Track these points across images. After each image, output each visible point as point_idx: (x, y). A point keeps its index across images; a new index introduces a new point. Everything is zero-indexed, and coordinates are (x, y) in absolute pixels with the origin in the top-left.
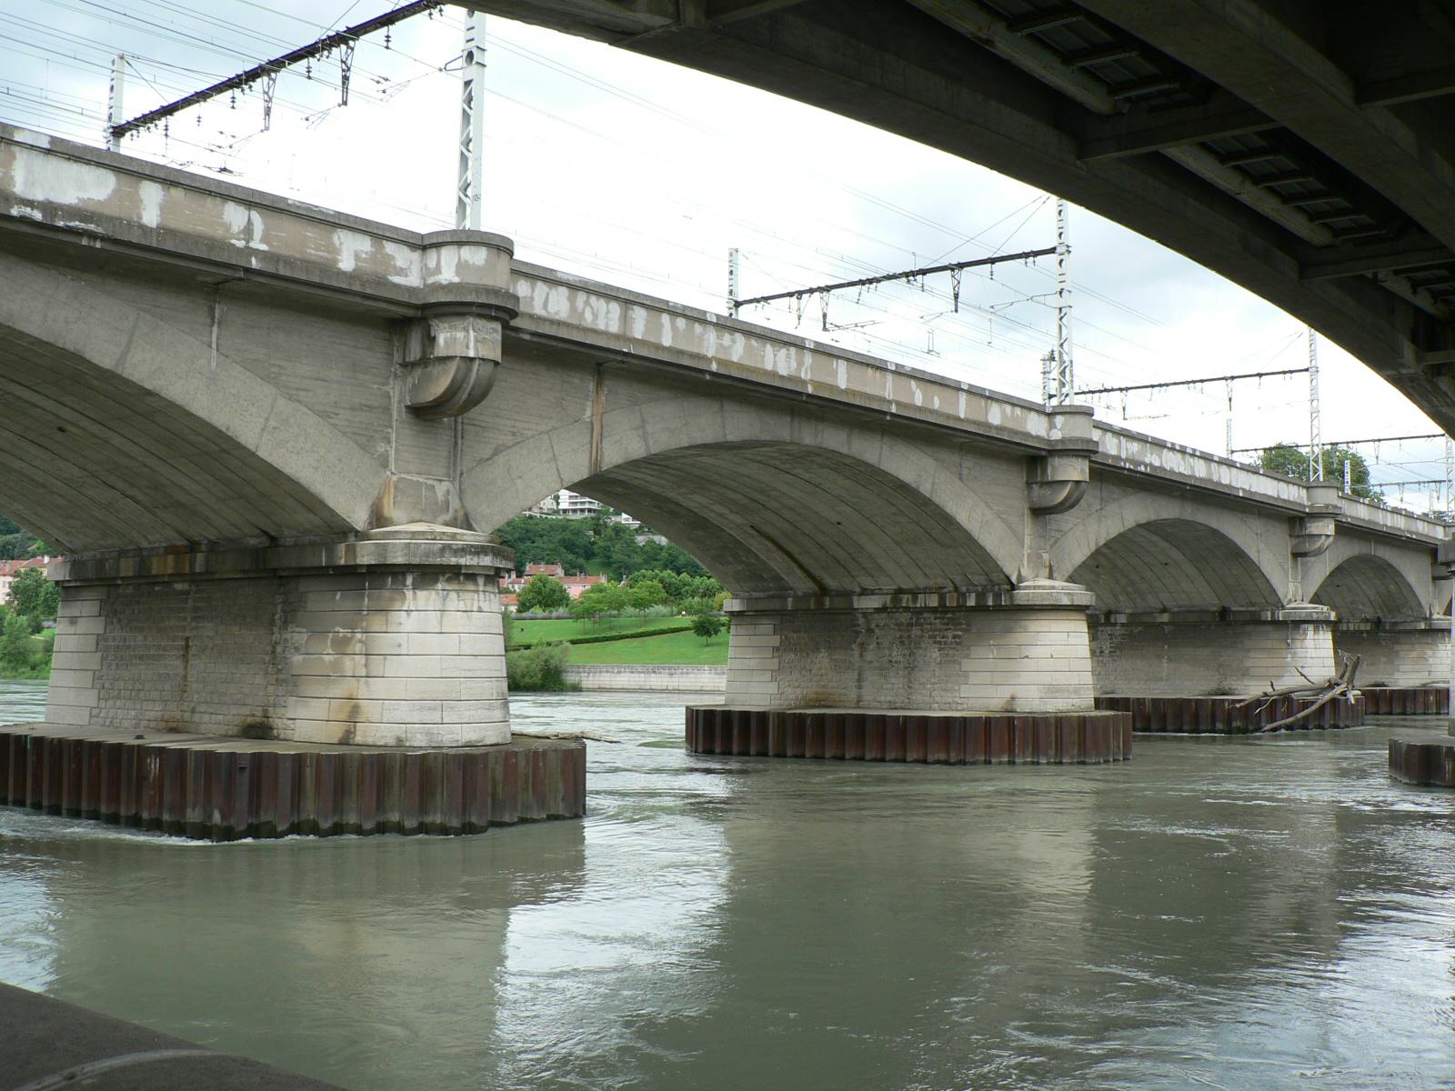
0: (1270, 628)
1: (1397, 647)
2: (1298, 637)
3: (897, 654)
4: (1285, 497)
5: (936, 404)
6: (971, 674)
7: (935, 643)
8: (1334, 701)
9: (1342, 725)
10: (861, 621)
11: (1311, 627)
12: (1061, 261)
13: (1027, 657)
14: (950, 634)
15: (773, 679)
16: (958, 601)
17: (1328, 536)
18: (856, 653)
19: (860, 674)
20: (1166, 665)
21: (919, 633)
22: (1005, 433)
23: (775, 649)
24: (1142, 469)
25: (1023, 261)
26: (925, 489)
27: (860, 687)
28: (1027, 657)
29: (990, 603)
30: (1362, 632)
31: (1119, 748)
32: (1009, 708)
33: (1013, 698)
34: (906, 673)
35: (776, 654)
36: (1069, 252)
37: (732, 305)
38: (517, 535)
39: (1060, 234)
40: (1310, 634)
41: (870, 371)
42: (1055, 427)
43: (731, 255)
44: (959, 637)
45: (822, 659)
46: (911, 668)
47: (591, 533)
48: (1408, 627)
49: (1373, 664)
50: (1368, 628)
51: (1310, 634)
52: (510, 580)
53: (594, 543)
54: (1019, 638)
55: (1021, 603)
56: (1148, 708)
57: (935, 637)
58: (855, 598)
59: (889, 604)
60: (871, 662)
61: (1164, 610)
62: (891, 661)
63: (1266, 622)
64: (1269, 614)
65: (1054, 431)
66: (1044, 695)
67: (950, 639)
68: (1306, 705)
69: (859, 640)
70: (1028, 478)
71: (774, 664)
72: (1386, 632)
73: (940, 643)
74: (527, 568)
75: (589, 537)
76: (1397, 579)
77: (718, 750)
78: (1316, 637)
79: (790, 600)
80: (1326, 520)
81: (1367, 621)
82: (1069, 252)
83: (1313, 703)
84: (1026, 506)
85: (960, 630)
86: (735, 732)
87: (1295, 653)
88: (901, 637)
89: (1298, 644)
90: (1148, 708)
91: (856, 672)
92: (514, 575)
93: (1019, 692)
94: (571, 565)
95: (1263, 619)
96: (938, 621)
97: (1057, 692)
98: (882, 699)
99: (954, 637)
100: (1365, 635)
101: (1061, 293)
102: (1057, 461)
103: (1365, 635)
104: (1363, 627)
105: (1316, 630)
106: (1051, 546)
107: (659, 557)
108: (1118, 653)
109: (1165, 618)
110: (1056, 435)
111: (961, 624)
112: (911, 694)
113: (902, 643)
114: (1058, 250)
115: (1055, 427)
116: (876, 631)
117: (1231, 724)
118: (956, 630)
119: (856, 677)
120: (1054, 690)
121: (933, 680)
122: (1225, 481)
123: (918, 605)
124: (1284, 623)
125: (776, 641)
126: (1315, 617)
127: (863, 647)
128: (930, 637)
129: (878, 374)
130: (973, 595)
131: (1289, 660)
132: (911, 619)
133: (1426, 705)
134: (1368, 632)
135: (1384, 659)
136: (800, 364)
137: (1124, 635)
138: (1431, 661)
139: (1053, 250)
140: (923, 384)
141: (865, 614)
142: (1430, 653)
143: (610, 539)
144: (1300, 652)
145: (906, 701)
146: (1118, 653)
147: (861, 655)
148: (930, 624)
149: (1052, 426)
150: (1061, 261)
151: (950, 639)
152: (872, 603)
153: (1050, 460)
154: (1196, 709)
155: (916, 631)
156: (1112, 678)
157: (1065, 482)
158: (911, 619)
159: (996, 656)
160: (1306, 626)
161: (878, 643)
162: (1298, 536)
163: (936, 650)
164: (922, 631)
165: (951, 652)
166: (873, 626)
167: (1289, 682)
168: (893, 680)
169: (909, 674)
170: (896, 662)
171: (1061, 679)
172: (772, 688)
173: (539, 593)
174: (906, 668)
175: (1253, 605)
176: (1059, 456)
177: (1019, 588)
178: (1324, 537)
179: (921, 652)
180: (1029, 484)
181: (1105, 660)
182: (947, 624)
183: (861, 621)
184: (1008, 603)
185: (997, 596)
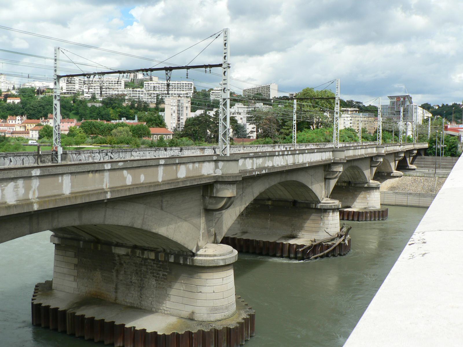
0: (314, 211)
1: (356, 193)
2: (326, 215)
3: (134, 279)
4: (324, 158)
5: (142, 179)
6: (171, 296)
7: (153, 276)
8: (340, 244)
9: (342, 254)
10: (117, 258)
11: (331, 211)
12: (225, 72)
13: (201, 292)
14: (161, 273)
15: (75, 280)
16: (165, 258)
17: (340, 172)
18: (114, 274)
19: (116, 285)
20: (269, 222)
21: (145, 270)
22: (188, 182)
23: (76, 265)
24: (264, 172)
25: (204, 69)
26: (138, 224)
27: (116, 292)
28: (201, 292)
29: (182, 262)
30: (343, 186)
31: (248, 334)
32: (191, 318)
33: (193, 313)
34: (139, 289)
35: (76, 268)
36: (229, 67)
37: (56, 77)
38: (45, 103)
39: (225, 44)
40: (331, 214)
41: (91, 175)
42: (218, 168)
43: (55, 50)
44: (165, 275)
45: (98, 275)
46: (141, 288)
47: (72, 102)
48: (360, 186)
49: (346, 199)
50: (346, 185)
51: (331, 214)
52: (42, 121)
53: (73, 106)
54: (197, 281)
55: (198, 265)
56: (262, 245)
57: (153, 273)
58: (113, 247)
59: (130, 253)
60: (121, 280)
61: (269, 199)
62: (131, 282)
63: (313, 208)
64: (314, 205)
65: (217, 170)
66: (209, 312)
67: (161, 276)
68: (328, 247)
69: (115, 268)
70: (203, 193)
71: (75, 273)
72: (352, 187)
73: (156, 277)
74: (49, 116)
75: (71, 104)
76: (359, 170)
77: (43, 326)
78: (333, 215)
79: (81, 242)
80: (340, 165)
81: (345, 182)
82: (229, 67)
83: (331, 246)
84: (202, 207)
85: (167, 272)
86: (51, 318)
87: (324, 222)
88: (136, 270)
89: (326, 218)
90: (262, 245)
91: (115, 284)
92: (43, 119)
93: (197, 310)
94: (65, 114)
95: (311, 207)
96: (155, 265)
97: (216, 310)
98: (128, 301)
99: (163, 275)
100: (344, 187)
101: (224, 90)
102: (219, 186)
103: (344, 187)
104: (343, 184)
105: (333, 212)
106: (216, 223)
107: (96, 111)
108: (249, 215)
109: (270, 203)
110: (219, 173)
111: (166, 269)
112: (141, 301)
113: (137, 273)
114: (224, 66)
115: (218, 168)
116: (124, 265)
117: (297, 255)
118: (164, 272)
119: (114, 286)
120: (215, 309)
121: (152, 296)
122: (301, 162)
123: (145, 257)
124: (320, 209)
125: (75, 261)
126: (333, 207)
127: (118, 272)
128: (151, 273)
129: (97, 175)
130: (173, 256)
131: (322, 225)
132: (142, 261)
133: (366, 217)
134: (345, 186)
135: (350, 197)
136: (28, 189)
137: (252, 208)
138: (368, 199)
139: (220, 65)
140: (132, 171)
141: (119, 256)
142: (368, 196)
143: (79, 105)
144: (326, 222)
145: (139, 304)
146: (249, 215)
147: (117, 276)
148: (151, 266)
149: (217, 167)
150: (225, 72)
151: (161, 276)
152: (121, 251)
153: (215, 185)
154: (282, 246)
155: (144, 269)
156: (247, 226)
157: (223, 198)
158: (142, 261)
159: (184, 289)
160: (329, 211)
161: (125, 271)
162: (328, 171)
163: (154, 280)
164: (147, 269)
165: (162, 283)
166: (122, 262)
167: (321, 236)
168: (133, 292)
169: (141, 290)
170: (134, 283)
171: (218, 303)
172: (74, 285)
173: (46, 132)
174: (139, 287)
175: (307, 200)
176: (220, 184)
177: (197, 255)
178: (338, 172)
179: (146, 280)
180: (203, 196)
181: (244, 218)
182: (160, 267)
183: (117, 258)
184: (191, 264)
185: (185, 259)
